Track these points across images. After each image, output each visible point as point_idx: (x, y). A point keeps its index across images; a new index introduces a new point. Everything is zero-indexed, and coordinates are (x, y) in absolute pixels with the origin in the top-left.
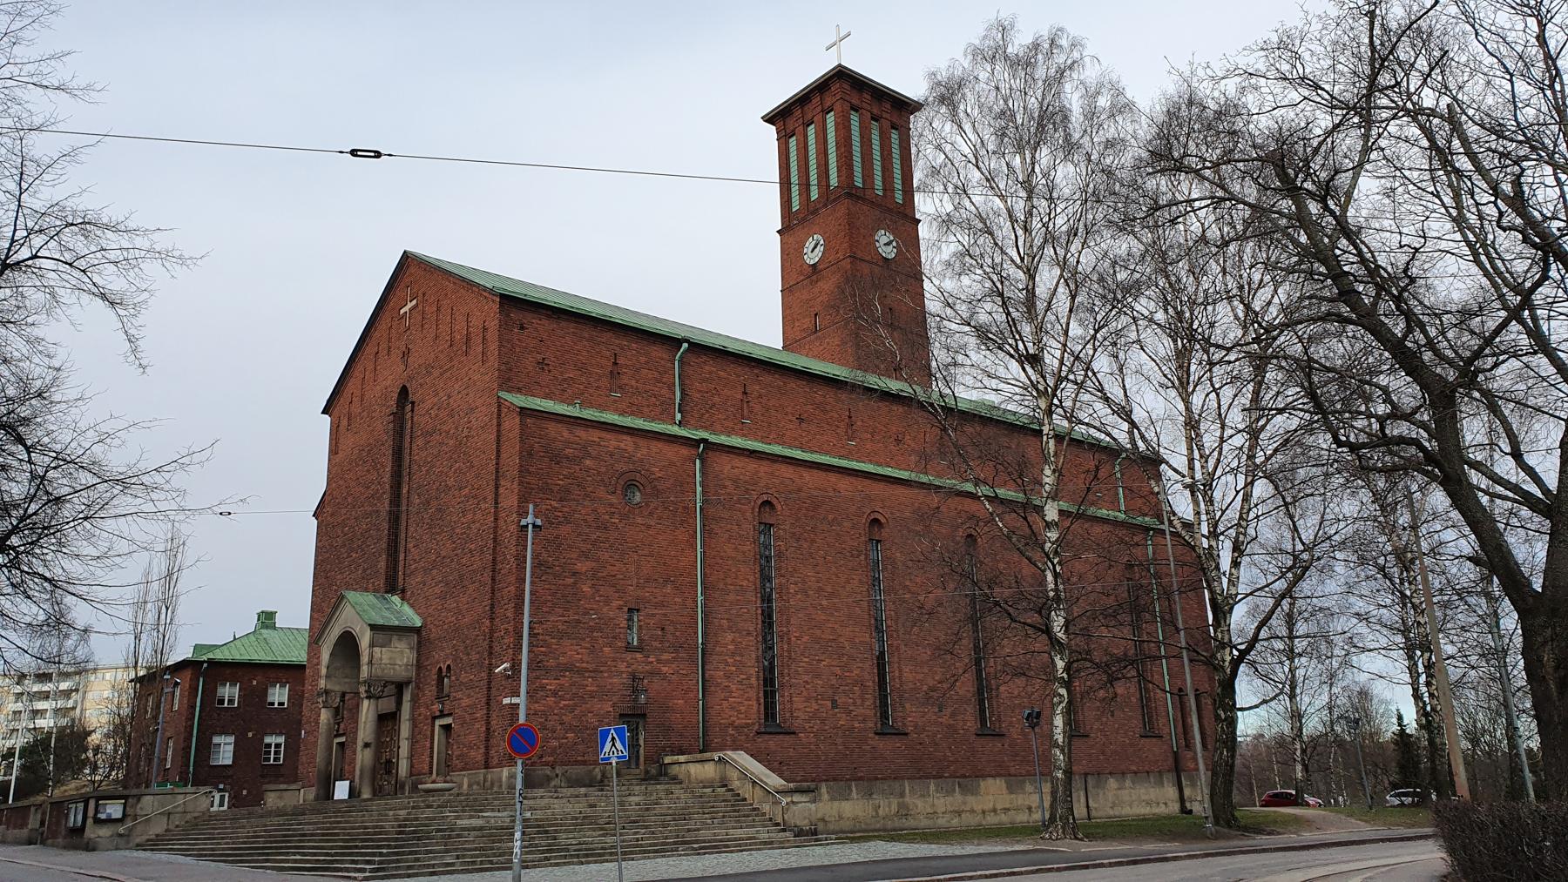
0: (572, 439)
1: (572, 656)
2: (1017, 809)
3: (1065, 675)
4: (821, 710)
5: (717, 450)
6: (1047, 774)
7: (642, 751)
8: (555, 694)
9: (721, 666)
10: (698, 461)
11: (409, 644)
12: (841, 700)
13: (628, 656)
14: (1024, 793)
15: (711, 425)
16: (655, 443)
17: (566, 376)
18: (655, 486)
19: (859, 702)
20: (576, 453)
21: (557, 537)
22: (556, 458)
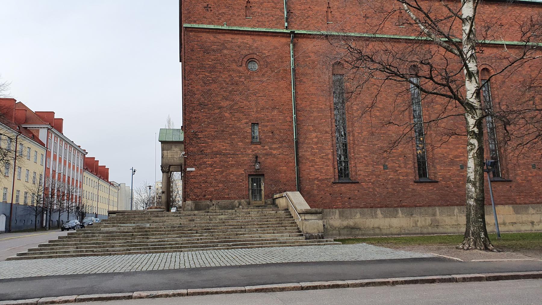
0: (216, 40)
1: (219, 148)
2: (522, 223)
3: (476, 130)
4: (376, 170)
5: (304, 37)
6: (462, 203)
7: (263, 192)
8: (211, 166)
9: (309, 150)
10: (291, 44)
11: (181, 149)
12: (389, 164)
13: (253, 146)
14: (528, 214)
15: (308, 27)
16: (265, 38)
17: (220, 12)
18: (266, 60)
19: (402, 165)
20: (219, 47)
21: (210, 90)
22: (207, 51)
